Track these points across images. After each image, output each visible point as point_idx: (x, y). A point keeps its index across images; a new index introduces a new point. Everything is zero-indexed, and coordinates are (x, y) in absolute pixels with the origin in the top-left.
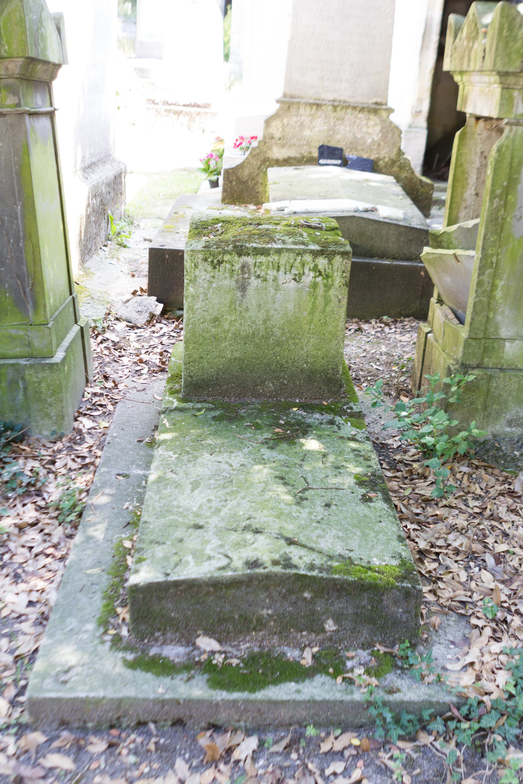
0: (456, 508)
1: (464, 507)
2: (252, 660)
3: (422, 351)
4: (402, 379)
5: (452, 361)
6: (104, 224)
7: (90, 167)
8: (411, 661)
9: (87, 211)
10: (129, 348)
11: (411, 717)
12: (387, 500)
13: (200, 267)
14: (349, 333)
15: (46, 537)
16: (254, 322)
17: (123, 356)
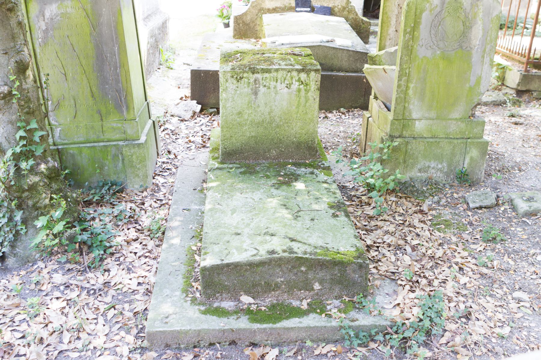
0: (388, 221)
1: (393, 221)
2: (273, 307)
3: (365, 129)
4: (354, 146)
5: (384, 134)
6: (157, 55)
7: (147, 18)
8: (364, 304)
10: (181, 134)
11: (365, 334)
12: (347, 216)
13: (229, 81)
14: (320, 119)
15: (144, 247)
16: (263, 114)
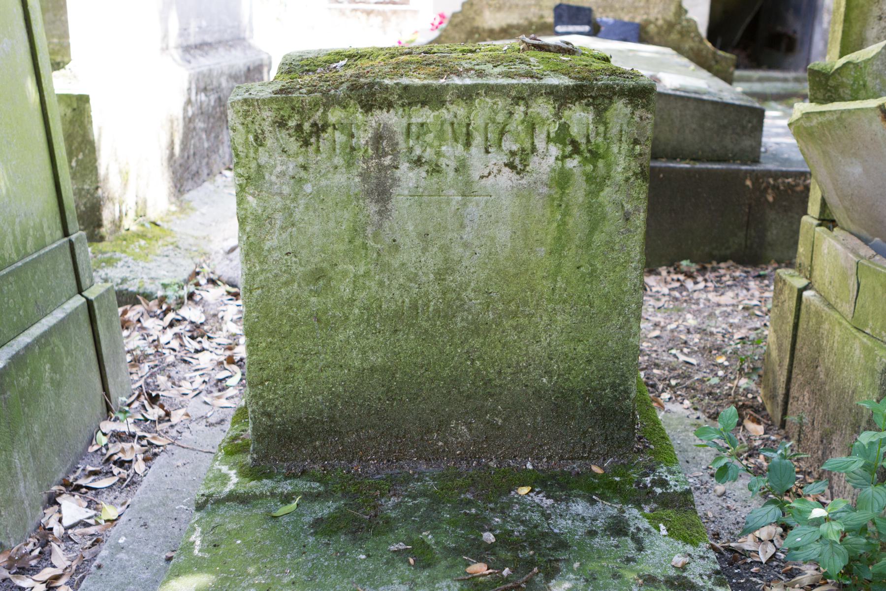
3: (789, 328)
9: (185, 110)
13: (269, 142)
16: (413, 278)
17: (203, 350)
